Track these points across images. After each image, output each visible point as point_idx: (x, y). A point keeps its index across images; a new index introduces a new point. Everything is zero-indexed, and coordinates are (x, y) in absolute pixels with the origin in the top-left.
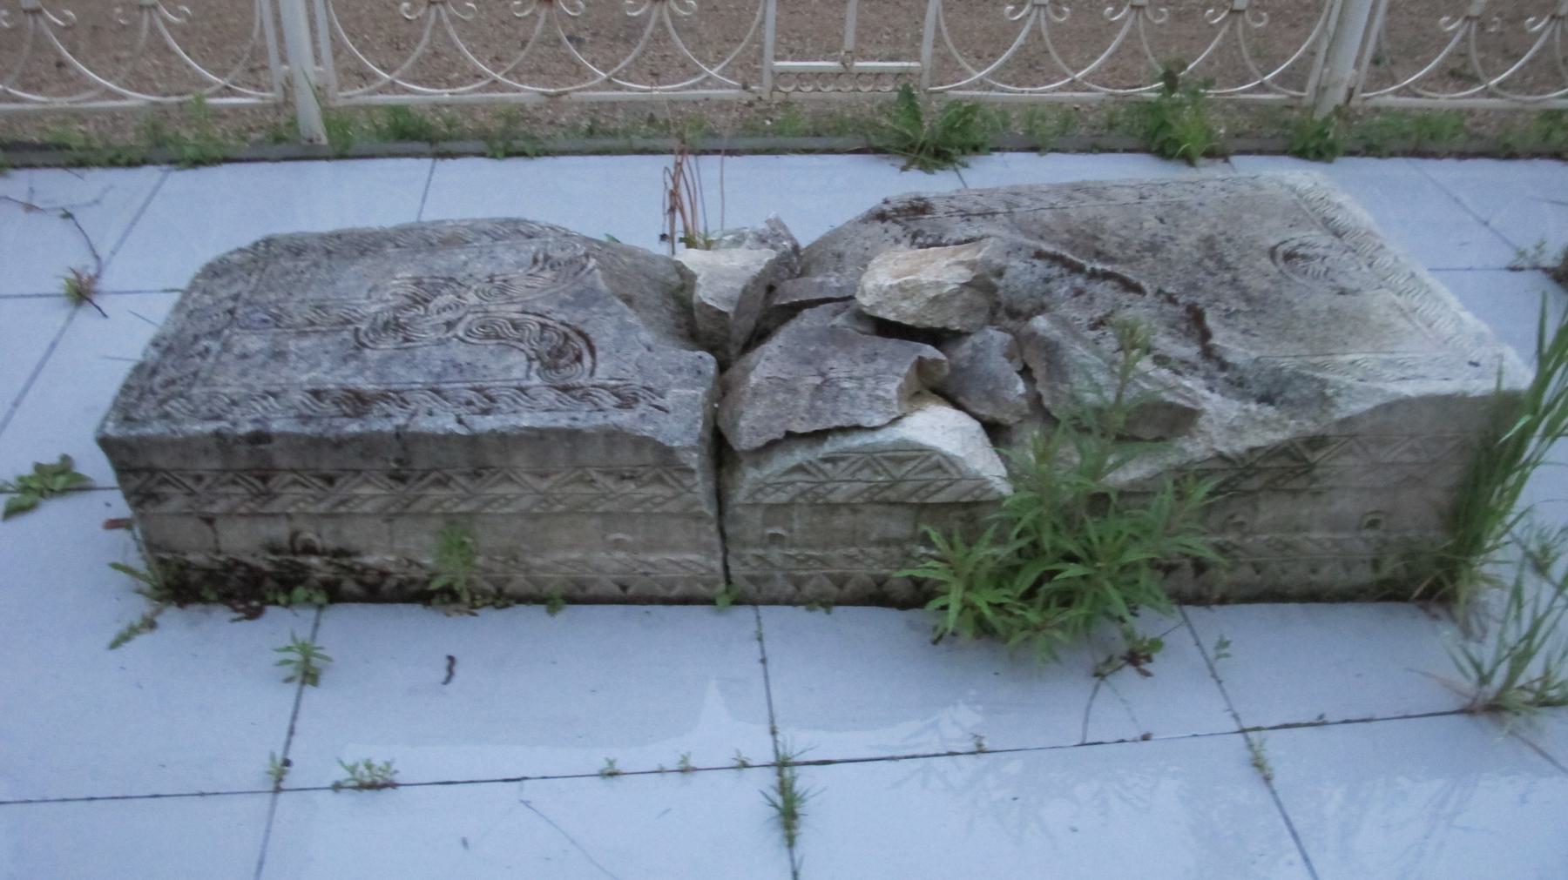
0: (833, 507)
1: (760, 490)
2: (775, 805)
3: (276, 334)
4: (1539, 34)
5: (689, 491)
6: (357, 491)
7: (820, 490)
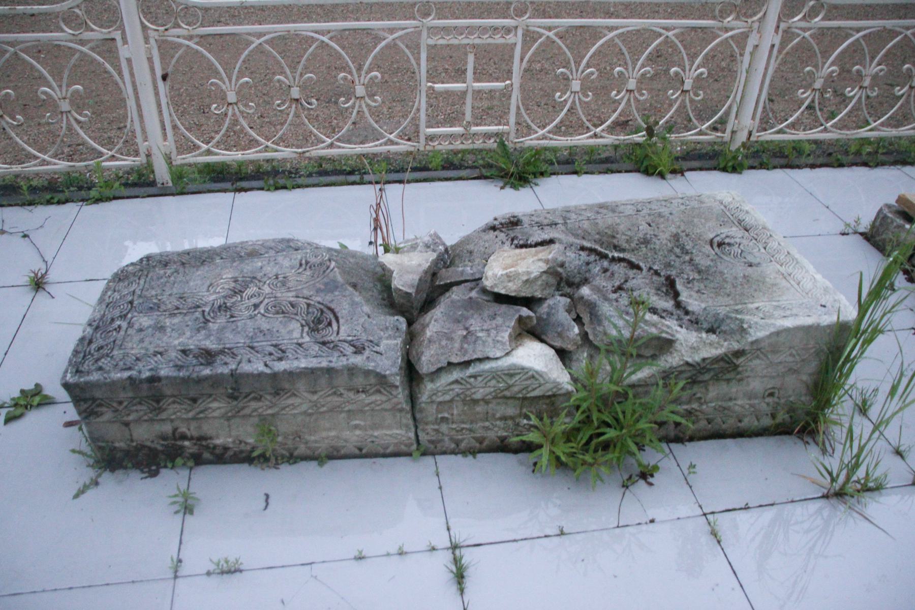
0: (475, 402)
1: (434, 394)
2: (452, 572)
3: (158, 316)
4: (853, 97)
5: (396, 397)
6: (211, 405)
7: (468, 393)
